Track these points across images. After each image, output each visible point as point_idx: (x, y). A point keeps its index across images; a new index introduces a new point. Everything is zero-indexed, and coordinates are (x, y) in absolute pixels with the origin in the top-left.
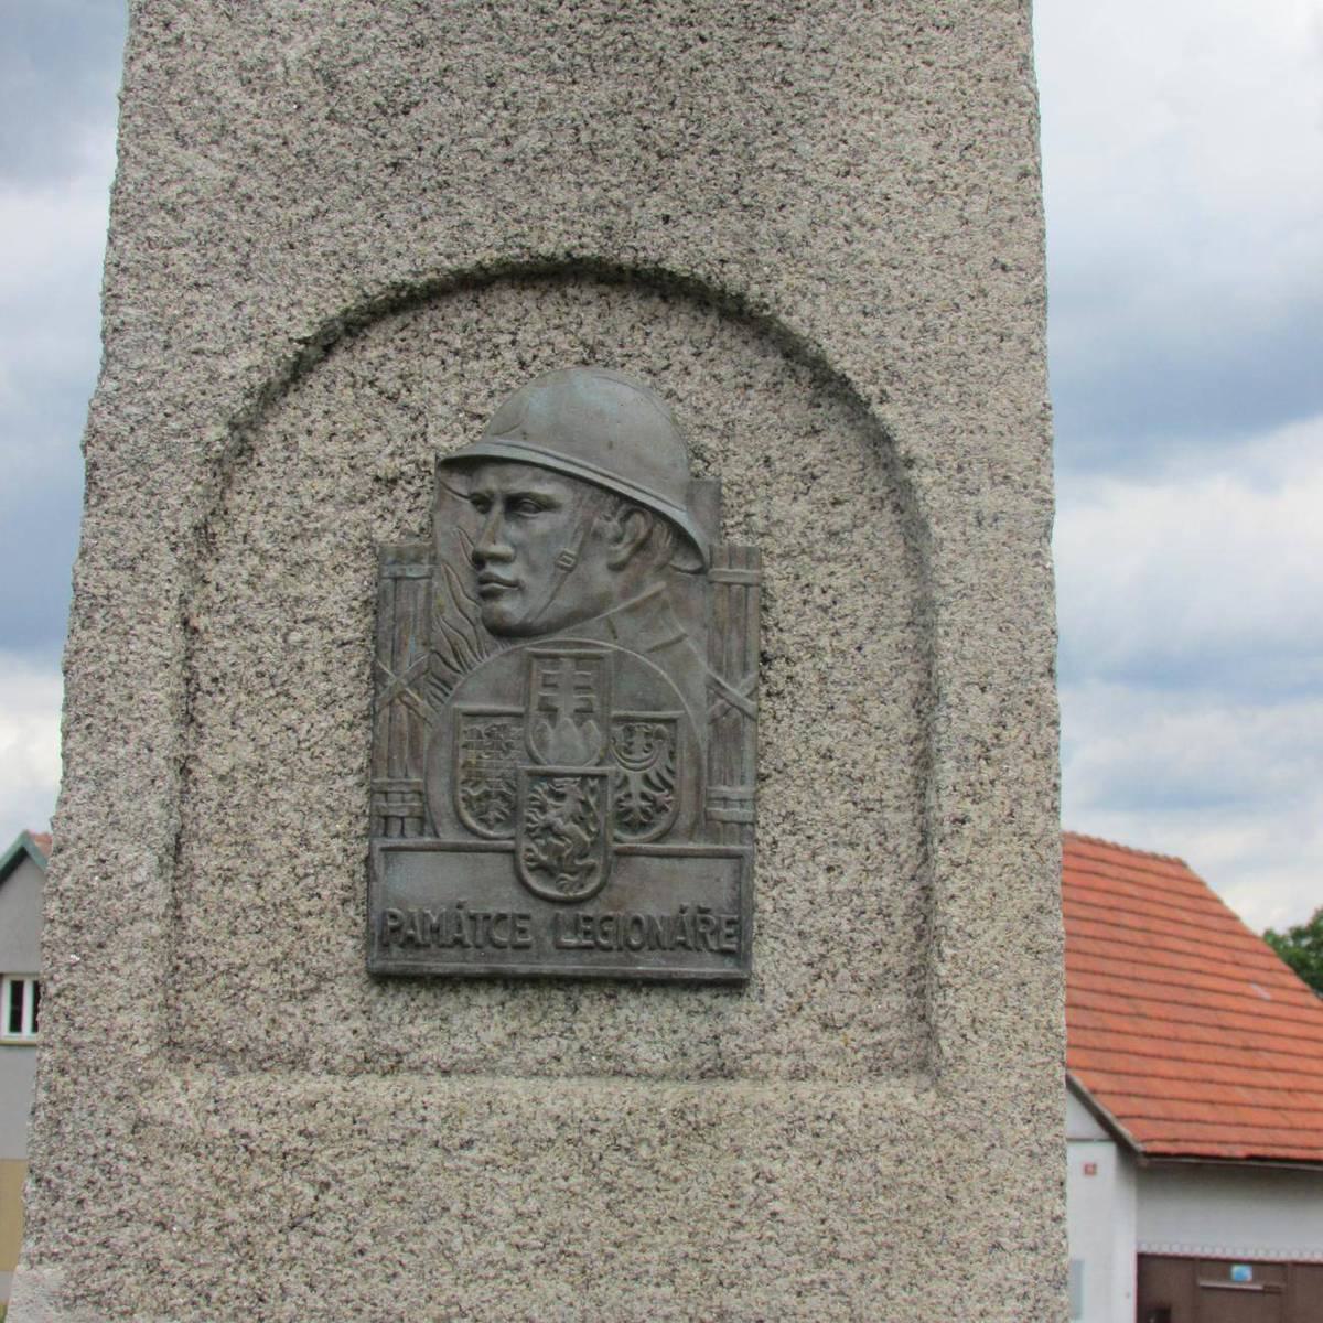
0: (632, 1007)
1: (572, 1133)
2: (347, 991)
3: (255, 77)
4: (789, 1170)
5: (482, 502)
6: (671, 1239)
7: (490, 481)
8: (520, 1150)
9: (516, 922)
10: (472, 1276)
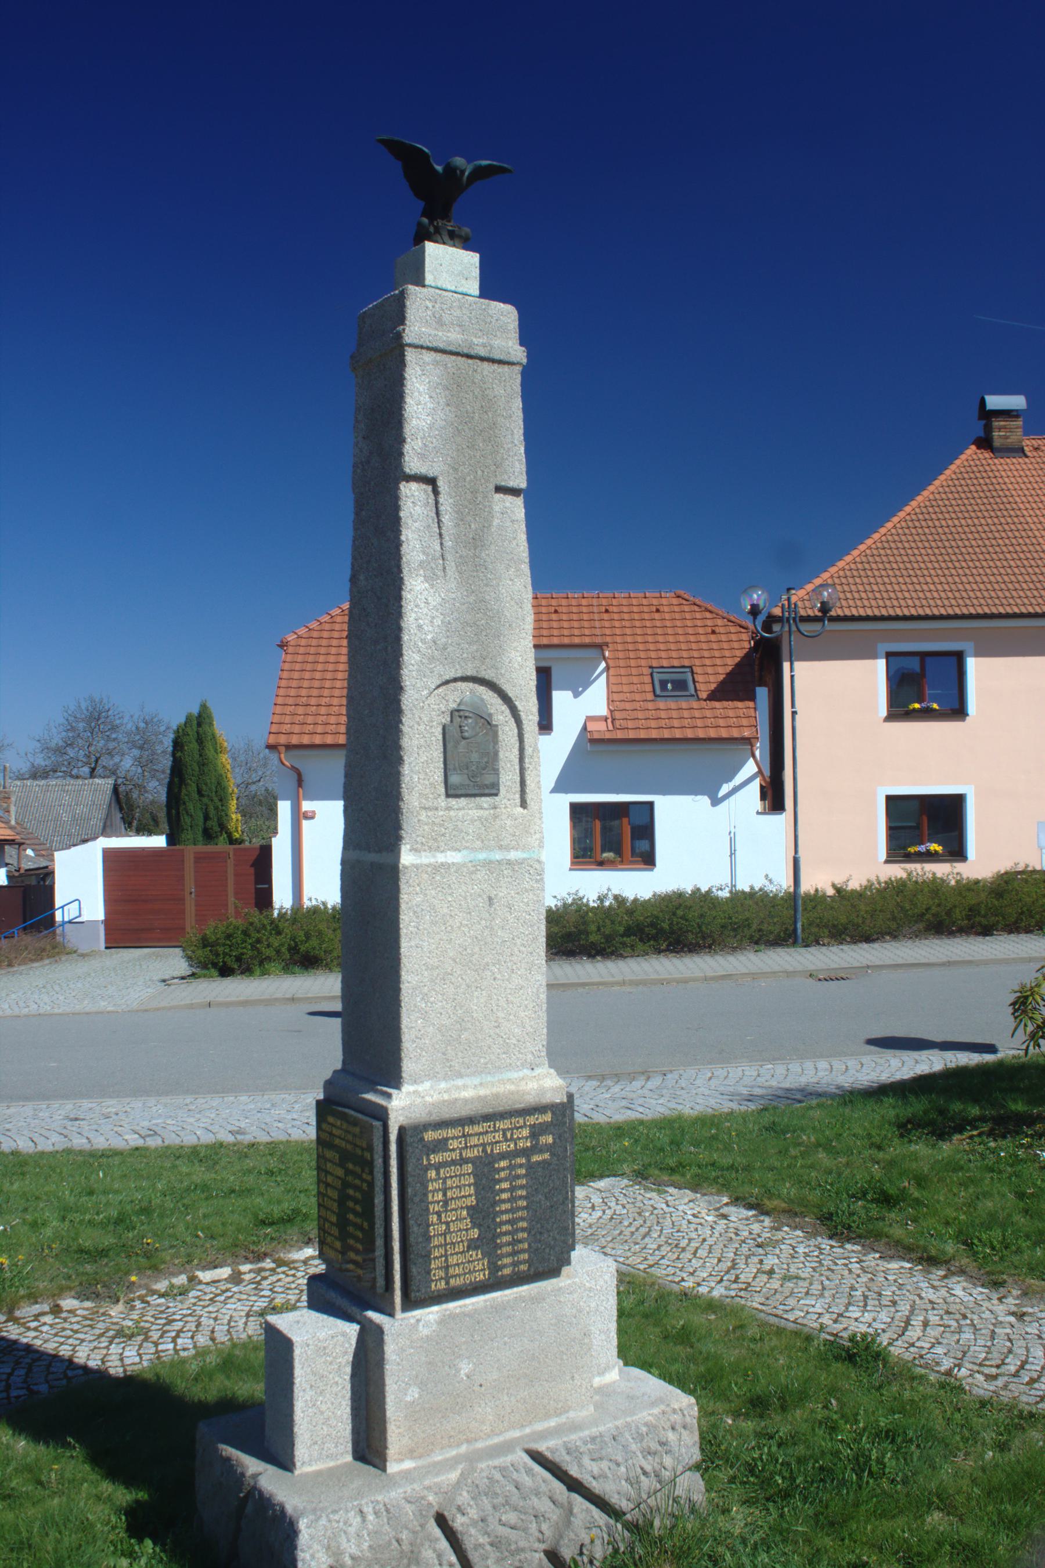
0: (483, 799)
1: (480, 818)
2: (443, 797)
3: (424, 641)
4: (508, 822)
5: (460, 717)
6: (494, 834)
7: (462, 713)
8: (473, 821)
9: (468, 785)
10: (467, 842)
